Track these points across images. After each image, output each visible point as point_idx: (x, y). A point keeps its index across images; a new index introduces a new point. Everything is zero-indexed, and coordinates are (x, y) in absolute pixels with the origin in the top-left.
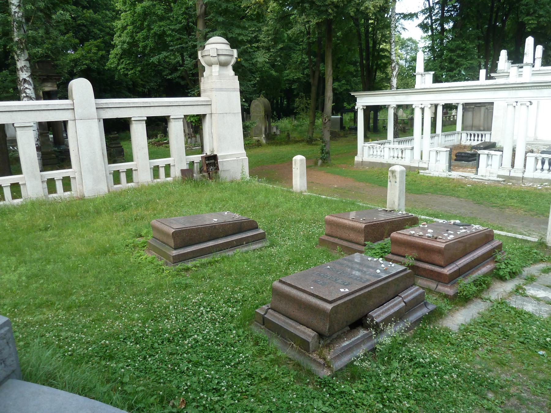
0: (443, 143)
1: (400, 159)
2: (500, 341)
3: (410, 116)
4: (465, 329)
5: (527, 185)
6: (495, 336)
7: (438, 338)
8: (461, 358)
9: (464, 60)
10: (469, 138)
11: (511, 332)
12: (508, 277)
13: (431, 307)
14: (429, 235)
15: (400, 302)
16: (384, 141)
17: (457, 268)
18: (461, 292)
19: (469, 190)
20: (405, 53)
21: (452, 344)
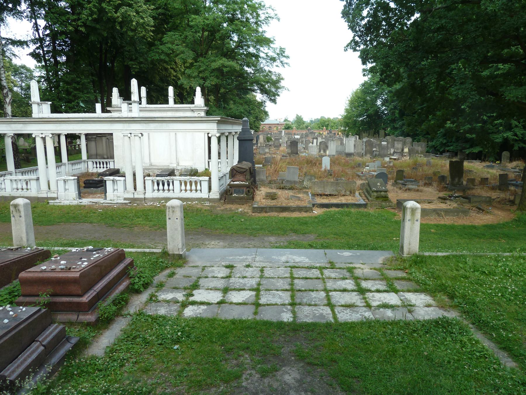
0: (71, 171)
1: (25, 190)
2: (143, 350)
3: (33, 146)
4: (110, 351)
5: (149, 204)
6: (138, 347)
7: (85, 370)
8: (110, 381)
9: (81, 94)
10: (95, 165)
11: (151, 338)
12: (142, 290)
13: (74, 341)
14: (62, 267)
15: (38, 348)
16: (4, 172)
17: (95, 293)
18: (102, 315)
19: (100, 215)
20: (19, 80)
21: (100, 371)
